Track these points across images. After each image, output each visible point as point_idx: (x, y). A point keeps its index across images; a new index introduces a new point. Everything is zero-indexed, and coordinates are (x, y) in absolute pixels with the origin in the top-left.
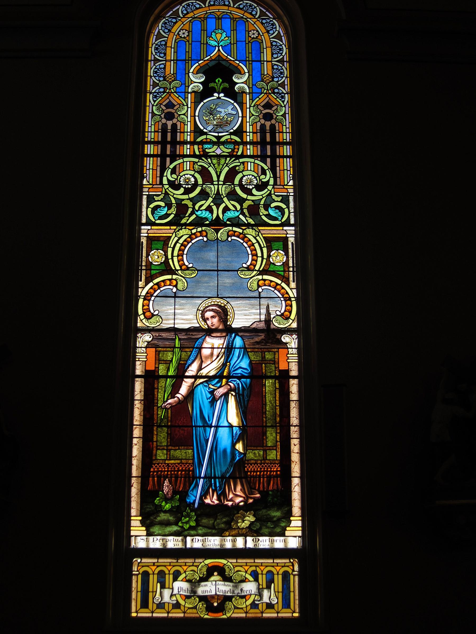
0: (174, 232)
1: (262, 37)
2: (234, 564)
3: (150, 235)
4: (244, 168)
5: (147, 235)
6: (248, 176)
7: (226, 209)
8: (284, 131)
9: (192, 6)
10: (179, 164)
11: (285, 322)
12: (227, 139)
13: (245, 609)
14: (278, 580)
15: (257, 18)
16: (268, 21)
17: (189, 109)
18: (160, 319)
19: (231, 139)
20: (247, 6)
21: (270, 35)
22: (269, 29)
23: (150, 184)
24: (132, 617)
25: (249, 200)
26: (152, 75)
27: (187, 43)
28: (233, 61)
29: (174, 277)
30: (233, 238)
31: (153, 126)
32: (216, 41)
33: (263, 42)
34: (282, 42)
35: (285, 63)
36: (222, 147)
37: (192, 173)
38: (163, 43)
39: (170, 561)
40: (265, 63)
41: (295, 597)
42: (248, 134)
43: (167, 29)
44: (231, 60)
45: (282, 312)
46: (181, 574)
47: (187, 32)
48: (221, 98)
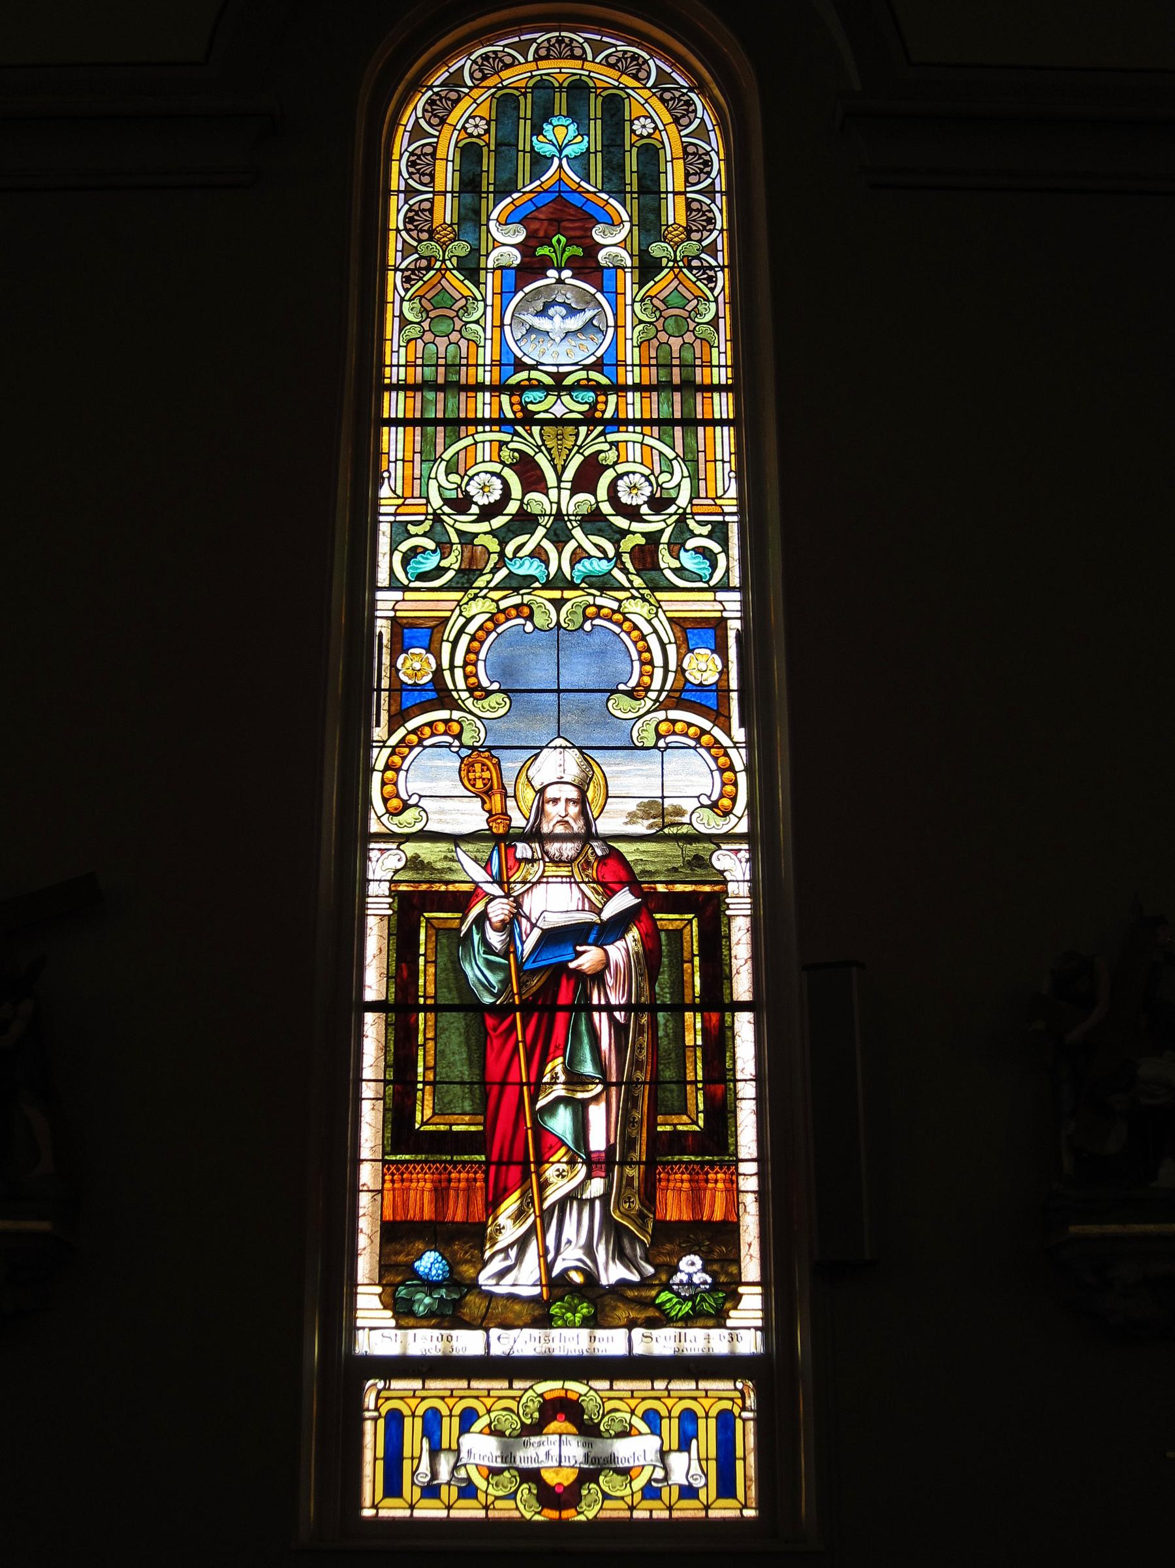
0: (458, 605)
1: (664, 133)
2: (602, 1394)
3: (399, 614)
4: (618, 456)
5: (392, 614)
6: (631, 475)
7: (579, 555)
8: (715, 362)
9: (494, 59)
10: (466, 448)
11: (720, 821)
12: (578, 381)
13: (629, 1500)
14: (708, 1432)
15: (649, 89)
16: (677, 94)
17: (489, 309)
18: (423, 813)
19: (588, 380)
20: (626, 59)
21: (680, 128)
22: (679, 115)
23: (399, 497)
24: (364, 1517)
25: (634, 533)
26: (401, 227)
27: (485, 150)
28: (594, 193)
29: (456, 715)
30: (597, 622)
31: (403, 350)
32: (553, 145)
33: (664, 148)
34: (710, 144)
35: (718, 196)
36: (566, 399)
37: (497, 467)
38: (428, 150)
39: (452, 1387)
40: (670, 196)
41: (746, 1468)
42: (629, 368)
43: (435, 116)
44: (588, 192)
45: (714, 798)
46: (479, 1417)
47: (484, 122)
48: (567, 281)
